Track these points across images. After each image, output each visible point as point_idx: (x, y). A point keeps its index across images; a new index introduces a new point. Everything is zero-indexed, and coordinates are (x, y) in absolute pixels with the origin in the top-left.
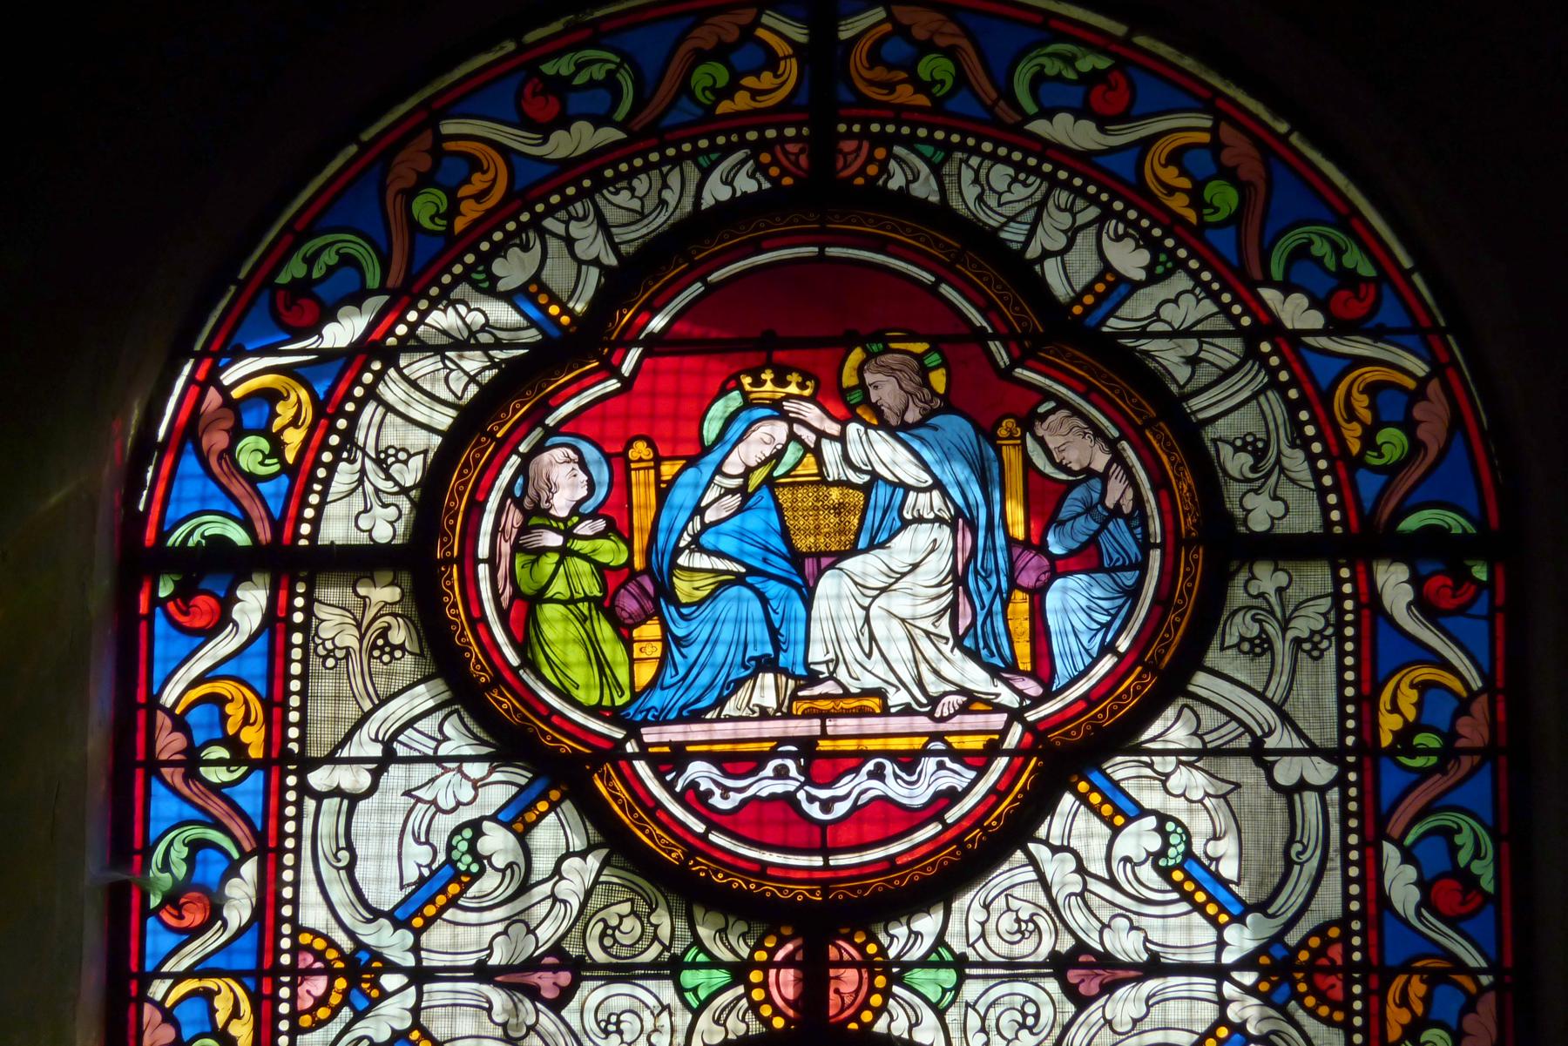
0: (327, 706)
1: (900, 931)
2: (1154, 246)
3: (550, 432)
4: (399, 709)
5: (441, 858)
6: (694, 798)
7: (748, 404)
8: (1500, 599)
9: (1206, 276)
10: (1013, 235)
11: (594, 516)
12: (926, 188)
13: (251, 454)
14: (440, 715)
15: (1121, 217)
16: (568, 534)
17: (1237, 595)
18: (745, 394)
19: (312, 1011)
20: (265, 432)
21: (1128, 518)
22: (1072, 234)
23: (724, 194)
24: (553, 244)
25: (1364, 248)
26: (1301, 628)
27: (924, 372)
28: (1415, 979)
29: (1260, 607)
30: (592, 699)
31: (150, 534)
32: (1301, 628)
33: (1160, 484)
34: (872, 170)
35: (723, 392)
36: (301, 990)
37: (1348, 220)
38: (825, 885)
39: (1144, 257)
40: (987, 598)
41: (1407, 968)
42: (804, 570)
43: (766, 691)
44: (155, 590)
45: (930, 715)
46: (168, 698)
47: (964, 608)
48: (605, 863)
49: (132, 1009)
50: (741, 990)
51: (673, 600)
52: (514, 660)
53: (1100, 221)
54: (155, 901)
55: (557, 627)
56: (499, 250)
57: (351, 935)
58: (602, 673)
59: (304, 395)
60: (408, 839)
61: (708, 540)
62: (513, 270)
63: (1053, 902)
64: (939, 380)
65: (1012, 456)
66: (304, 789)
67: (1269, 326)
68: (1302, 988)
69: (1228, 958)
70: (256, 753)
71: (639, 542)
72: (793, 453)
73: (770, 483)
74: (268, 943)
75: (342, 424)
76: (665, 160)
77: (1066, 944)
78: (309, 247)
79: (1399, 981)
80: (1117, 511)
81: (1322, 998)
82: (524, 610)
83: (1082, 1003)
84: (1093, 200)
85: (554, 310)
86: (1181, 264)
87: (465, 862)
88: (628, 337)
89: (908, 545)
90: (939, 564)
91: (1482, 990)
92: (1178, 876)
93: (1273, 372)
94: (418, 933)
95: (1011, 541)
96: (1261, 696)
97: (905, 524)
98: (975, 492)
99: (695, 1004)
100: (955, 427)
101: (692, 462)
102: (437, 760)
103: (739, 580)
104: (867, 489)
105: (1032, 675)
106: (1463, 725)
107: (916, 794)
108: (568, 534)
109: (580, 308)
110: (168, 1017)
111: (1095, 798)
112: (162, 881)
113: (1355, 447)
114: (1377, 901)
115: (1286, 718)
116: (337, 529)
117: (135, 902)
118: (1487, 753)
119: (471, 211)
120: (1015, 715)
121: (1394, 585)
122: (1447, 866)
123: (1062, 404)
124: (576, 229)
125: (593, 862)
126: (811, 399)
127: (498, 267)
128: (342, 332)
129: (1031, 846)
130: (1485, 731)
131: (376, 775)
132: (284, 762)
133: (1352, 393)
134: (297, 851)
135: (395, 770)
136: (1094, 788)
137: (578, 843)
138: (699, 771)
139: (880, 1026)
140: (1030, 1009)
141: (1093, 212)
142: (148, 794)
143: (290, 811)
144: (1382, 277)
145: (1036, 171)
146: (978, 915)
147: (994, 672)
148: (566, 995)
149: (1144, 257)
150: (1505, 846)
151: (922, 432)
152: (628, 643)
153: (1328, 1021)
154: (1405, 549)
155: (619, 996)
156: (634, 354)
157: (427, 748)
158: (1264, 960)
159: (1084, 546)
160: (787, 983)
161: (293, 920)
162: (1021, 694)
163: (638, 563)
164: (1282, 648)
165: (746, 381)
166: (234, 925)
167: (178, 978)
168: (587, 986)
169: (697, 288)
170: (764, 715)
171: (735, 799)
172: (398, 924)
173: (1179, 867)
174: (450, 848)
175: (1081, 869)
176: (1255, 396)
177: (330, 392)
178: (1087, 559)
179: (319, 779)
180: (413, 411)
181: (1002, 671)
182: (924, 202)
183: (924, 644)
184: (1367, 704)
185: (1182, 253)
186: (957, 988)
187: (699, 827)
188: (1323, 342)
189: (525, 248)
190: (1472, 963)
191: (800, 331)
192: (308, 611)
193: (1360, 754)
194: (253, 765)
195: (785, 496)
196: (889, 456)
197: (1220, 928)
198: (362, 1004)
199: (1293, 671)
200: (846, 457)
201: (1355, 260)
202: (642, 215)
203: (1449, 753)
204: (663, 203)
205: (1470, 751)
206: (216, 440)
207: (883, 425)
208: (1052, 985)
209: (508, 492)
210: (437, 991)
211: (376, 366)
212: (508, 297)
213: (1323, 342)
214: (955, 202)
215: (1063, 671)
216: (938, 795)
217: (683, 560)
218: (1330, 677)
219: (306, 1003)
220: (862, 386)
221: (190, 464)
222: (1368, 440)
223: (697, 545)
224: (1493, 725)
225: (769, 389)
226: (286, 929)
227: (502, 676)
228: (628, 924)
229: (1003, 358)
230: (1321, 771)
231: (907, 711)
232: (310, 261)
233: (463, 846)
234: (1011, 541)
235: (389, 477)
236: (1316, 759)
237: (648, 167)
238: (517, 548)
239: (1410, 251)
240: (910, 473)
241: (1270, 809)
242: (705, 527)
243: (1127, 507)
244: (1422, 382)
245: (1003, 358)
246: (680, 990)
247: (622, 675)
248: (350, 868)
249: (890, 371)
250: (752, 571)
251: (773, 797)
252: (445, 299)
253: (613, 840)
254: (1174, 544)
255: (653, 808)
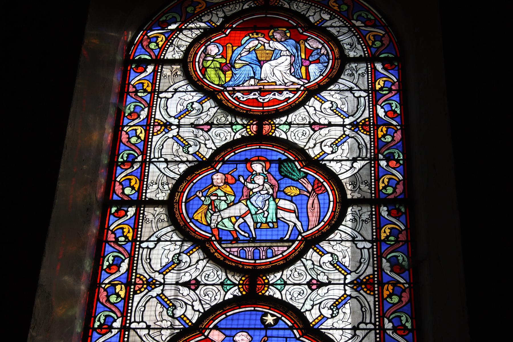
0: (146, 231)
1: (272, 276)
2: (331, 15)
3: (211, 43)
4: (164, 231)
5: (185, 108)
6: (237, 99)
7: (250, 38)
8: (400, 67)
9: (341, 19)
10: (299, 306)
11: (219, 55)
12: (278, 295)
13: (153, 46)
14: (172, 233)
15: (325, 10)
16: (214, 58)
17: (347, 67)
18: (250, 37)
19: (157, 132)
20: (156, 42)
21: (325, 55)
22: (313, 306)
23: (240, 137)
24: (214, 15)
25: (372, 15)
26: (360, 72)
27: (285, 33)
28: (390, 285)
29: (352, 69)
30: (217, 83)
31: (131, 58)
32: (360, 72)
33: (332, 50)
34: (276, 4)
35: (246, 36)
36: (155, 129)
37: (369, 11)
38: (263, 112)
39: (329, 16)
40: (297, 67)
41: (388, 283)
42: (261, 63)
43: (252, 82)
44: (111, 211)
45: (285, 86)
46: (132, 83)
47: (292, 68)
48: (207, 262)
49: (120, 132)
50: (245, 129)
51: (234, 67)
52: (202, 77)
53: (320, 11)
54: (126, 115)
55: (211, 73)
56: (203, 16)
57: (149, 275)
58: (219, 79)
59: (164, 37)
60: (179, 104)
61: (242, 58)
62: (206, 18)
63: (309, 115)
64: (288, 35)
65: (303, 46)
66: (374, 324)
67: (354, 26)
68: (361, 129)
69: (347, 281)
70: (130, 239)
71: (228, 59)
72: (259, 45)
73: (254, 50)
74: (126, 305)
75: (171, 41)
76: (236, 2)
77: (312, 121)
78: (166, 15)
79: (386, 286)
80: (323, 54)
81: (365, 130)
82: (204, 70)
83: (315, 131)
84: (319, 8)
85: (213, 24)
86: (337, 17)
87: (176, 261)
88: (207, 327)
89: (283, 59)
90: (288, 62)
91: (406, 288)
92: (335, 111)
93: (354, 33)
94: (164, 275)
95: (302, 59)
96: (352, 83)
97: (281, 56)
98: (295, 51)
99: (226, 290)
100: (292, 42)
101: (239, 47)
102: (170, 241)
103: (248, 65)
104: (274, 51)
105: (306, 79)
106: (400, 236)
107: (281, 98)
108: (214, 58)
109: (218, 24)
110: (127, 133)
111: (318, 99)
112: (127, 112)
113: (371, 44)
114: (380, 269)
115: (357, 86)
116: (169, 56)
117: (123, 114)
118: (406, 242)
119: (198, 10)
120: (302, 86)
121: (379, 66)
122: (400, 324)
123: (312, 38)
124: (218, 13)
125: (216, 108)
126: (263, 37)
127: (203, 18)
128: (173, 27)
129: (302, 259)
130: (405, 237)
131: (156, 245)
132: (155, 92)
133: (370, 37)
134: (375, 311)
135: (177, 94)
136: (318, 248)
137: (213, 106)
138: (239, 95)
139: (267, 294)
140: (304, 132)
141: (319, 10)
142: (127, 97)
143: (155, 100)
144: (376, 19)
145: (308, 4)
146: (218, 297)
147: (298, 79)
148: (209, 130)
149: (329, 16)
150: (414, 320)
151: (286, 42)
152: (225, 75)
153: (366, 134)
154: (380, 60)
155: (219, 130)
156: (229, 31)
157: (168, 239)
158: (355, 282)
159: (316, 60)
160: (254, 128)
161: (154, 118)
162: (304, 82)
163: (228, 62)
164: (356, 75)
165: (251, 35)
166: (121, 272)
167: (131, 126)
168: (213, 129)
169: (242, 21)
170: (252, 85)
171: (245, 99)
172: (160, 273)
173: (335, 109)
174: (187, 106)
175: (315, 110)
176: (351, 37)
177: (168, 36)
178: (317, 61)
179: (144, 245)
180: (185, 39)
181: (300, 78)
182: (287, 8)
183: (284, 74)
184: (373, 83)
185: (336, 15)
186: (289, 129)
187: (238, 103)
188: (364, 28)
189: (208, 15)
190: (402, 282)
191: (262, 27)
192: (162, 69)
193: (376, 241)
194: (149, 93)
195: (258, 52)
196: (278, 46)
197: (344, 119)
198: (150, 289)
199: (358, 79)
200: (270, 46)
201: (370, 16)
202: (231, 11)
203: (397, 241)
204: (235, 9)
205: (394, 90)
206: (145, 43)
207: (277, 41)
208: (309, 128)
209: (203, 51)
210: (166, 287)
211: (178, 32)
212: (205, 23)
213: (364, 28)
214: (284, 298)
215: (312, 80)
216: (286, 98)
217: (236, 62)
218: (366, 80)
219: (155, 131)
220: (273, 35)
221: (140, 47)
222: (373, 43)
223: (239, 59)
224: (407, 236)
225: (255, 36)
226: (153, 119)
227: (200, 79)
228: (222, 119)
229: (301, 31)
230: (364, 94)
231: (280, 85)
232: (166, 17)
233: (335, 312)
234: (302, 59)
235: (179, 49)
236: (367, 243)
237: (233, 4)
238: (204, 60)
239: (381, 15)
240: (283, 49)
241: (354, 100)
242: (241, 57)
243: (325, 53)
244: (384, 35)
245: (301, 31)
246: (232, 129)
247: (223, 79)
248: (166, 110)
249: (279, 33)
250: (250, 63)
251: (253, 98)
252: (193, 22)
253: (220, 105)
254: (334, 59)
255: (229, 100)
